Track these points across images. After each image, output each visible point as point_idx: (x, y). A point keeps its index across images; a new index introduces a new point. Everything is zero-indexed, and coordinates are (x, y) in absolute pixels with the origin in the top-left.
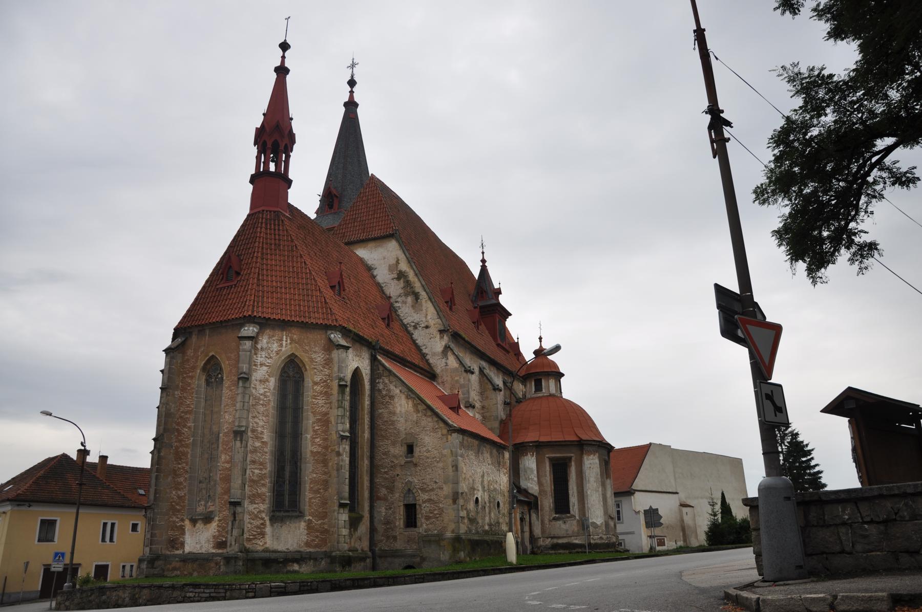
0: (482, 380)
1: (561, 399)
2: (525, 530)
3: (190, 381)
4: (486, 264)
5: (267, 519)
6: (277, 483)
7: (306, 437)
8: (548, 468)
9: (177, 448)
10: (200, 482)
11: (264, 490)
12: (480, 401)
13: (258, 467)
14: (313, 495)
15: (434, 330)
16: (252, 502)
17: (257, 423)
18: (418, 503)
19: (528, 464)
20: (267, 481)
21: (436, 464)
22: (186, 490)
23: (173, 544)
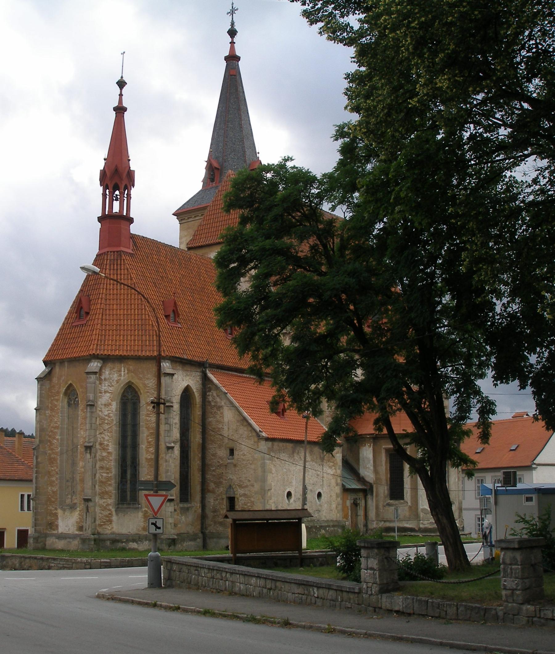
2: (359, 514)
5: (113, 510)
7: (142, 447)
9: (50, 455)
10: (67, 481)
11: (111, 488)
13: (106, 471)
16: (102, 498)
17: (103, 438)
19: (366, 453)
20: (113, 482)
21: (249, 466)
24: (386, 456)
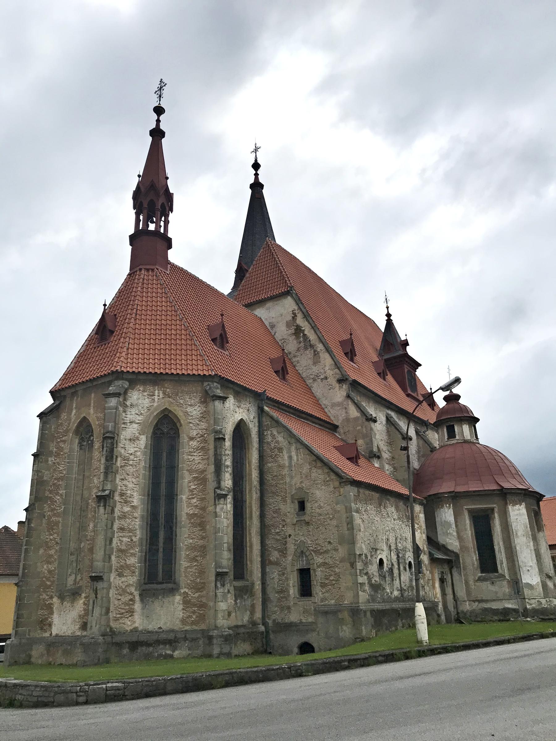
0: (389, 430)
1: (477, 445)
2: (447, 592)
3: (63, 446)
4: (391, 318)
5: (136, 594)
6: (150, 551)
7: (182, 498)
8: (468, 521)
10: (72, 554)
12: (390, 452)
14: (189, 564)
15: (332, 381)
16: (120, 575)
18: (311, 567)
20: (137, 550)
21: (329, 522)
22: (56, 564)
23: (42, 625)
24: (470, 519)
